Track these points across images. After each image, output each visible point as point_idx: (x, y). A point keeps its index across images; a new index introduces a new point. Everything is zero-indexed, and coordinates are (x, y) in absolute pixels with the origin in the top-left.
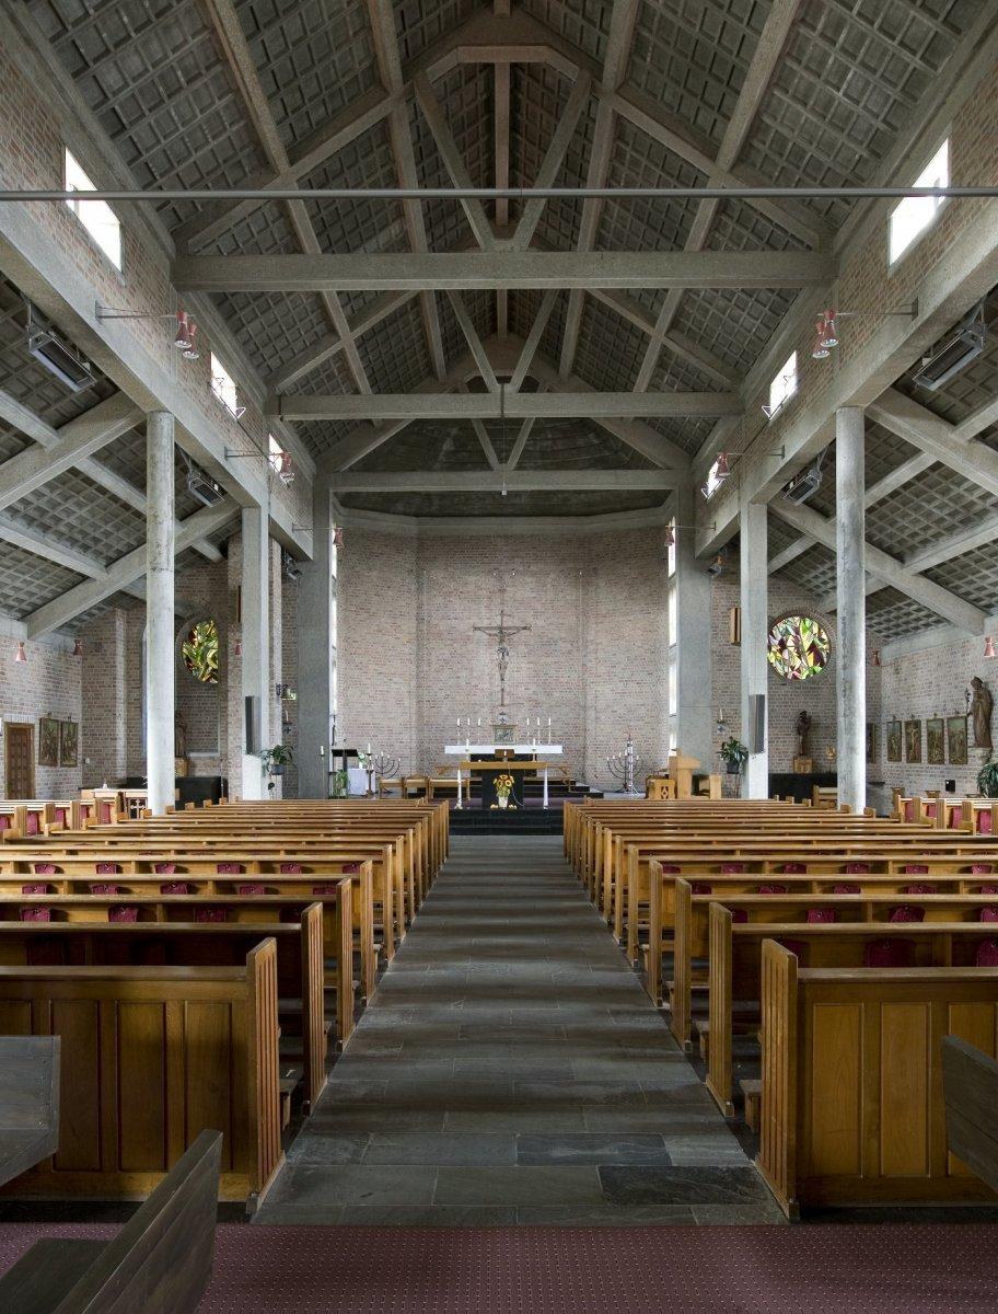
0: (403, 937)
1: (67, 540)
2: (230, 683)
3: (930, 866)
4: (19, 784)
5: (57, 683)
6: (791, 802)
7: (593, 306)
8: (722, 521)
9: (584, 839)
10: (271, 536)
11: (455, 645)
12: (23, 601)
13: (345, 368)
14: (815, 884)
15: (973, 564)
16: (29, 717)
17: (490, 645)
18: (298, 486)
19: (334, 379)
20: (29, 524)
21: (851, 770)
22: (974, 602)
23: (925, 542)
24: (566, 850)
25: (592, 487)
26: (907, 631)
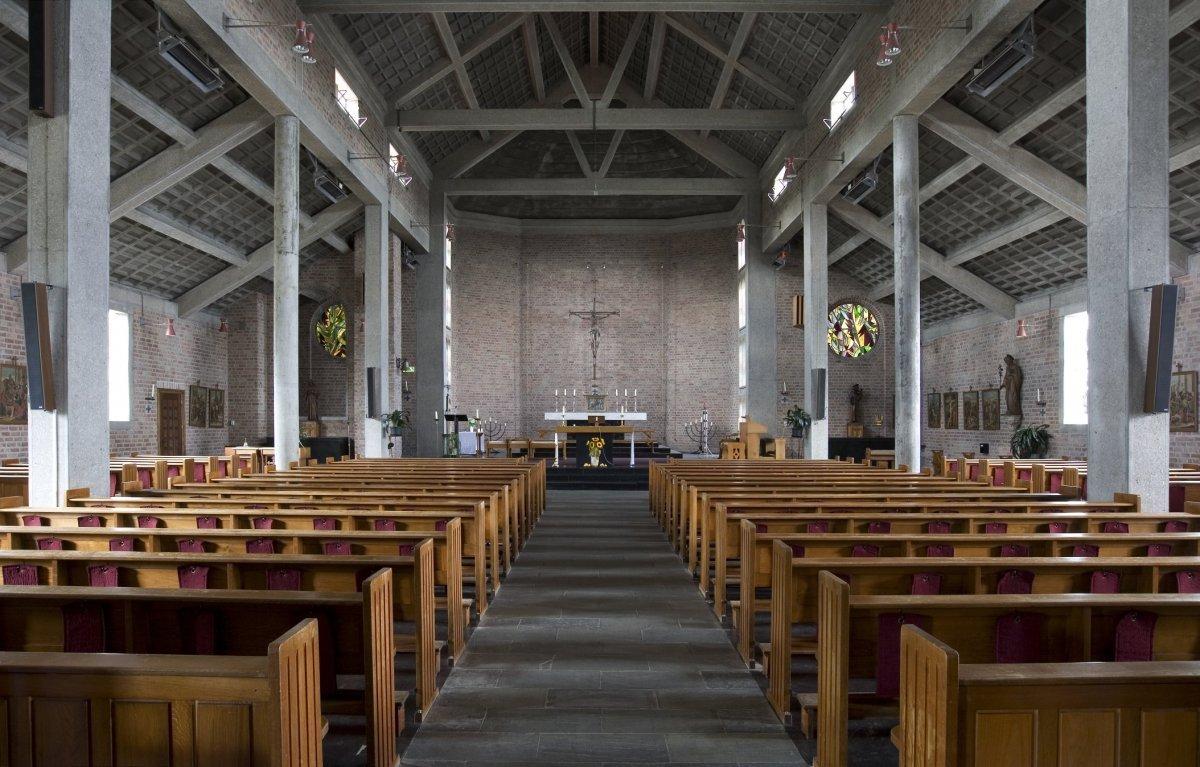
0: (497, 589)
1: (210, 231)
2: (356, 357)
3: (1008, 523)
4: (171, 441)
5: (205, 356)
6: (851, 462)
7: (672, 48)
8: (787, 221)
9: (668, 499)
10: (391, 230)
11: (554, 327)
12: (174, 284)
13: (456, 89)
14: (909, 544)
15: (1007, 257)
16: (180, 384)
17: (583, 327)
18: (416, 187)
19: (448, 96)
20: (238, 247)
21: (908, 435)
22: (1006, 291)
23: (965, 238)
24: (651, 504)
25: (672, 193)
26: (945, 316)
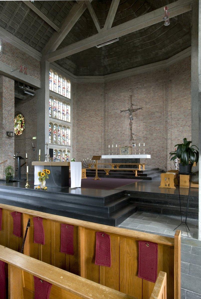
11: (117, 119)
